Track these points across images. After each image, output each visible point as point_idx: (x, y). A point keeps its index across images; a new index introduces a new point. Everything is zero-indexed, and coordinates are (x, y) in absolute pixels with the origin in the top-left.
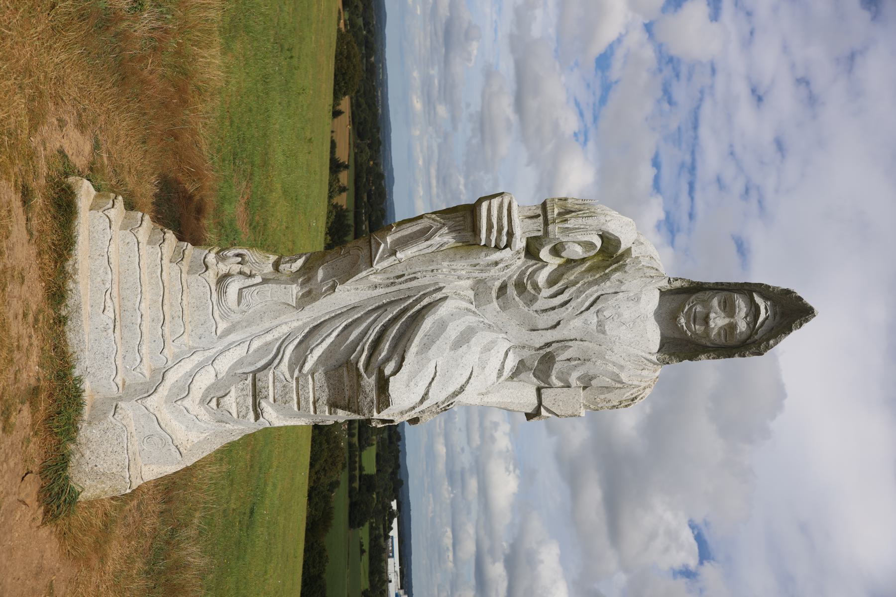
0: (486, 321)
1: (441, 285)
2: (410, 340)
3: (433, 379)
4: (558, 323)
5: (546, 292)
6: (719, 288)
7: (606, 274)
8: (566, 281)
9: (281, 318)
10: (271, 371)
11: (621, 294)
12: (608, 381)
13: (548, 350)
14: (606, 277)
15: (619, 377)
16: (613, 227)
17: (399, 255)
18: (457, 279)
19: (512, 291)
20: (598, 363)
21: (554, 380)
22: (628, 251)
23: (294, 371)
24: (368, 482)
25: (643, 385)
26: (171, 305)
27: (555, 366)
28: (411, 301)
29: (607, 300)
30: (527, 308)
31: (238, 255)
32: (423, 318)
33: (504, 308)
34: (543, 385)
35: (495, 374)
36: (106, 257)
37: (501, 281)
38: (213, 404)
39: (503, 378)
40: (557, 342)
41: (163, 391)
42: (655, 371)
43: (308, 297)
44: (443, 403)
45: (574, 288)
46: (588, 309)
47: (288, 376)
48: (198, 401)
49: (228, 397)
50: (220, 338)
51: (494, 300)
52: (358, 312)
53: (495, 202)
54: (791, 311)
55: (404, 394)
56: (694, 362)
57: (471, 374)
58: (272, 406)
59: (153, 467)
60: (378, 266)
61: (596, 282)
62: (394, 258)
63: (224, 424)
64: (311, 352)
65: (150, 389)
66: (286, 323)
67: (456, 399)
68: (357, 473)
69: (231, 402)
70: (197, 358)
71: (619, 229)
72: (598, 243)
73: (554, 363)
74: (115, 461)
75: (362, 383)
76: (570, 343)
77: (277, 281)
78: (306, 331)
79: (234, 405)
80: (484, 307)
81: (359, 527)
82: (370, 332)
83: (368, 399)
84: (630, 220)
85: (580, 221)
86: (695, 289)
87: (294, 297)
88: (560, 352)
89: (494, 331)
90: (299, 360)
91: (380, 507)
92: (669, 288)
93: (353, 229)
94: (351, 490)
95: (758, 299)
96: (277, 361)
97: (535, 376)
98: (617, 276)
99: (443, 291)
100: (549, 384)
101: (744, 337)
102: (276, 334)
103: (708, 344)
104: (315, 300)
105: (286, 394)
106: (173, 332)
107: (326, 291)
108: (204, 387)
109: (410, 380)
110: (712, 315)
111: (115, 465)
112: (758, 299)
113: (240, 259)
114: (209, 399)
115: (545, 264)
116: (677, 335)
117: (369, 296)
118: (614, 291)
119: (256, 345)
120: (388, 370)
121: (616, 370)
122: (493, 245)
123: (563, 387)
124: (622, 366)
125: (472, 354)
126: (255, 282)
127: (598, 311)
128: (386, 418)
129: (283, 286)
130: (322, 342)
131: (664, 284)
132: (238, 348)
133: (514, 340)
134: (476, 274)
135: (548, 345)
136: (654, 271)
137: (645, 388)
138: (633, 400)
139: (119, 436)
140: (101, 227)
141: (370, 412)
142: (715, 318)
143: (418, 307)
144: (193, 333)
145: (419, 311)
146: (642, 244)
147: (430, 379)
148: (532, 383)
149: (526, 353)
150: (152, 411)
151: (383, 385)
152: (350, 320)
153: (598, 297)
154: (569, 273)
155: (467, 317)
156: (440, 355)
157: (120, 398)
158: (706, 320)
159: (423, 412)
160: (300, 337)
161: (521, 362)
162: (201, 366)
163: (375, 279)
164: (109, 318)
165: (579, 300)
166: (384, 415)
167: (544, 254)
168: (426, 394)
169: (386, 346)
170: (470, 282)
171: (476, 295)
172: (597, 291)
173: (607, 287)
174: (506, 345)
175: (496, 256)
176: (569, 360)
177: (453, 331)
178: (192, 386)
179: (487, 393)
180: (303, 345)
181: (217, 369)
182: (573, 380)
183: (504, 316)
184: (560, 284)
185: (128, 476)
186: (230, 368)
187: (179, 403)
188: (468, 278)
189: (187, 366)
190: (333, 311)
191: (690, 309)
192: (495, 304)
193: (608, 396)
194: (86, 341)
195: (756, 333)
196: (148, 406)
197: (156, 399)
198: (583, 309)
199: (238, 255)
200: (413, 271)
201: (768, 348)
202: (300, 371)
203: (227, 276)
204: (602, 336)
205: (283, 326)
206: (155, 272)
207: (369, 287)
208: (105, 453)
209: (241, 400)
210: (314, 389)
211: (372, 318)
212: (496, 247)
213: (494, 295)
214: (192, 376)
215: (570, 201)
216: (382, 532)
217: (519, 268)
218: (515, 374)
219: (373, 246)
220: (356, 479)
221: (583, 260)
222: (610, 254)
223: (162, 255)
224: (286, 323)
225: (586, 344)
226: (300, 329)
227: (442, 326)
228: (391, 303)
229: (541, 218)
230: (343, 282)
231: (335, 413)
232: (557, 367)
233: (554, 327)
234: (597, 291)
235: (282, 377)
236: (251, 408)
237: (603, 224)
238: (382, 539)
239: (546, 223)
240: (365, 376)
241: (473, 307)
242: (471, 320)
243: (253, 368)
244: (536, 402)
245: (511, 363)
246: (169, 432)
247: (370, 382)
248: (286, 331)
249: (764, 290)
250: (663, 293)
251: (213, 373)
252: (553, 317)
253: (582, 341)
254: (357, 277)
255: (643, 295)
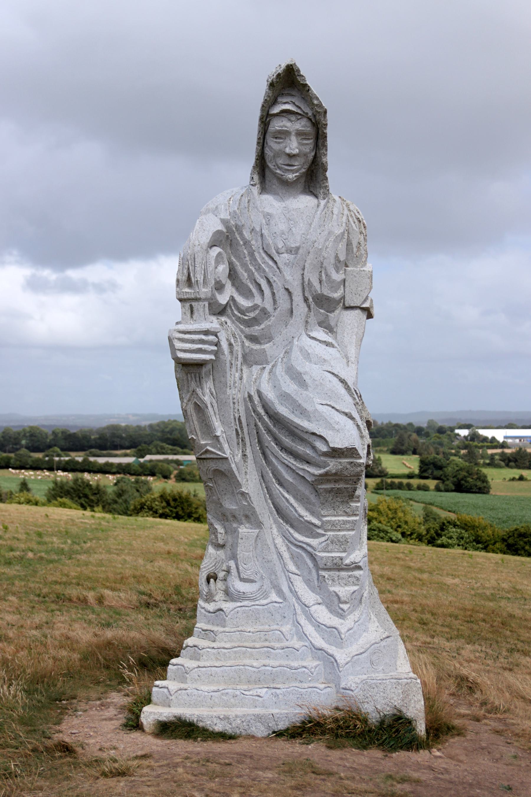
0: (282, 355)
1: (246, 395)
2: (297, 427)
3: (333, 407)
4: (287, 290)
5: (258, 300)
6: (262, 143)
7: (245, 244)
8: (248, 281)
9: (269, 543)
10: (318, 554)
11: (263, 231)
12: (342, 246)
13: (311, 300)
14: (246, 243)
15: (339, 236)
16: (204, 238)
17: (218, 433)
18: (243, 382)
19: (256, 330)
20: (326, 255)
21: (336, 295)
22: (224, 222)
23: (318, 533)
24: (429, 469)
25: (346, 212)
26: (254, 641)
27: (325, 294)
28: (259, 424)
29: (268, 245)
30: (272, 318)
31: (208, 582)
32: (277, 414)
33: (270, 339)
34: (341, 304)
35: (330, 350)
36: (213, 694)
37: (245, 340)
38: (345, 607)
39: (334, 342)
40: (304, 291)
41: (332, 650)
42: (334, 200)
43: (250, 517)
44: (354, 399)
45: (256, 274)
46: (276, 263)
47: (323, 539)
48: (341, 621)
49: (341, 594)
50: (285, 599)
51: (263, 347)
52: (267, 473)
53: (178, 345)
54: (288, 81)
55: (347, 434)
56: (328, 167)
57: (330, 372)
58: (349, 554)
59: (398, 663)
60: (228, 453)
61: (252, 254)
62: (221, 438)
63: (364, 598)
64: (302, 517)
65: (330, 661)
66: (274, 539)
67: (352, 387)
68: (415, 482)
69: (344, 591)
70: (303, 620)
71: (206, 232)
72: (217, 250)
73: (323, 295)
74: (392, 690)
75: (334, 471)
76: (306, 280)
77: (234, 546)
78: (282, 521)
79: (347, 588)
80: (269, 358)
81: (487, 482)
82: (286, 462)
83: (348, 466)
84: (198, 222)
85: (198, 269)
86: (262, 166)
87: (250, 531)
88: (313, 289)
89: (291, 349)
90: (309, 529)
91: (463, 452)
92: (258, 186)
93: (79, 475)
94: (438, 489)
95: (276, 110)
96: (309, 549)
97: (333, 311)
98: (247, 234)
99: (253, 394)
100: (341, 299)
101: (309, 124)
102: (283, 549)
103: (313, 154)
104: (254, 512)
105: (339, 541)
106: (279, 640)
107: (248, 502)
108: (329, 615)
109: (333, 429)
110: (288, 150)
111: (396, 691)
112: (276, 110)
113: (212, 580)
114: (340, 611)
115: (232, 299)
116: (303, 180)
117: (252, 462)
118: (259, 238)
119: (292, 567)
120: (324, 449)
121: (332, 239)
122: (215, 348)
123: (344, 286)
124: (329, 233)
125: (312, 371)
126: (234, 566)
127: (278, 253)
128: (365, 451)
129: (240, 541)
130: (293, 507)
131: (256, 190)
132: (295, 584)
133: (300, 331)
134: (239, 363)
135: (306, 300)
136: (243, 198)
137: (350, 210)
138: (360, 221)
139: (370, 686)
140: (186, 697)
141: (360, 465)
142: (291, 149)
143: (266, 418)
144: (280, 623)
145: (270, 417)
146: (217, 207)
147: (333, 410)
148: (339, 314)
149: (313, 320)
150: (349, 659)
151: (336, 453)
152: (274, 480)
153: (266, 252)
154: (242, 278)
155: (277, 373)
156: (313, 401)
157: (337, 685)
158: (291, 156)
159: (361, 417)
160: (288, 527)
161: (320, 324)
162: (310, 617)
163: (239, 457)
164: (267, 692)
165: (267, 270)
166: (363, 453)
167: (223, 299)
168: (346, 414)
169: (301, 449)
170: (244, 368)
171: (256, 363)
172: (259, 253)
173: (256, 244)
174: (304, 338)
175: (224, 345)
176: (320, 282)
177: (290, 387)
178: (328, 625)
179: (347, 358)
180: (295, 524)
181: (312, 603)
182: (337, 277)
183: (278, 339)
184: (251, 287)
185: (406, 680)
186: (313, 591)
187: (343, 636)
188: (242, 370)
189: (309, 629)
190: (265, 496)
191: (280, 168)
192: (266, 346)
193: (355, 244)
194: (286, 711)
195: (307, 114)
196: (345, 662)
197: (339, 655)
198: (275, 267)
199: (208, 582)
200: (233, 421)
201: (320, 105)
202: (319, 527)
203: (227, 592)
204: (301, 251)
205: (276, 542)
206: (224, 654)
207: (245, 461)
208: (384, 698)
209: (342, 582)
210: (335, 516)
211: (274, 460)
212: (216, 345)
213: (256, 347)
214: (318, 625)
215: (180, 278)
216: (499, 451)
217: (233, 322)
218: (330, 329)
219: (208, 456)
220: (432, 483)
221: (231, 264)
222: (227, 239)
223: (209, 648)
224: (274, 539)
225: (307, 265)
226: (279, 527)
227: (285, 397)
228: (260, 442)
229: (193, 304)
230: (239, 485)
231: (358, 497)
232: (326, 292)
233: (290, 293)
234: (259, 253)
235: (323, 544)
236: (350, 573)
237: (202, 248)
238: (507, 451)
239: (197, 300)
240: (328, 468)
241: (268, 367)
242: (280, 370)
243: (314, 572)
244: (358, 311)
245: (321, 334)
246: (368, 646)
247: (333, 465)
248: (281, 540)
249: (270, 102)
250: (264, 190)
251: (317, 606)
252: (281, 295)
253: (303, 269)
254: (236, 473)
255: (265, 210)
